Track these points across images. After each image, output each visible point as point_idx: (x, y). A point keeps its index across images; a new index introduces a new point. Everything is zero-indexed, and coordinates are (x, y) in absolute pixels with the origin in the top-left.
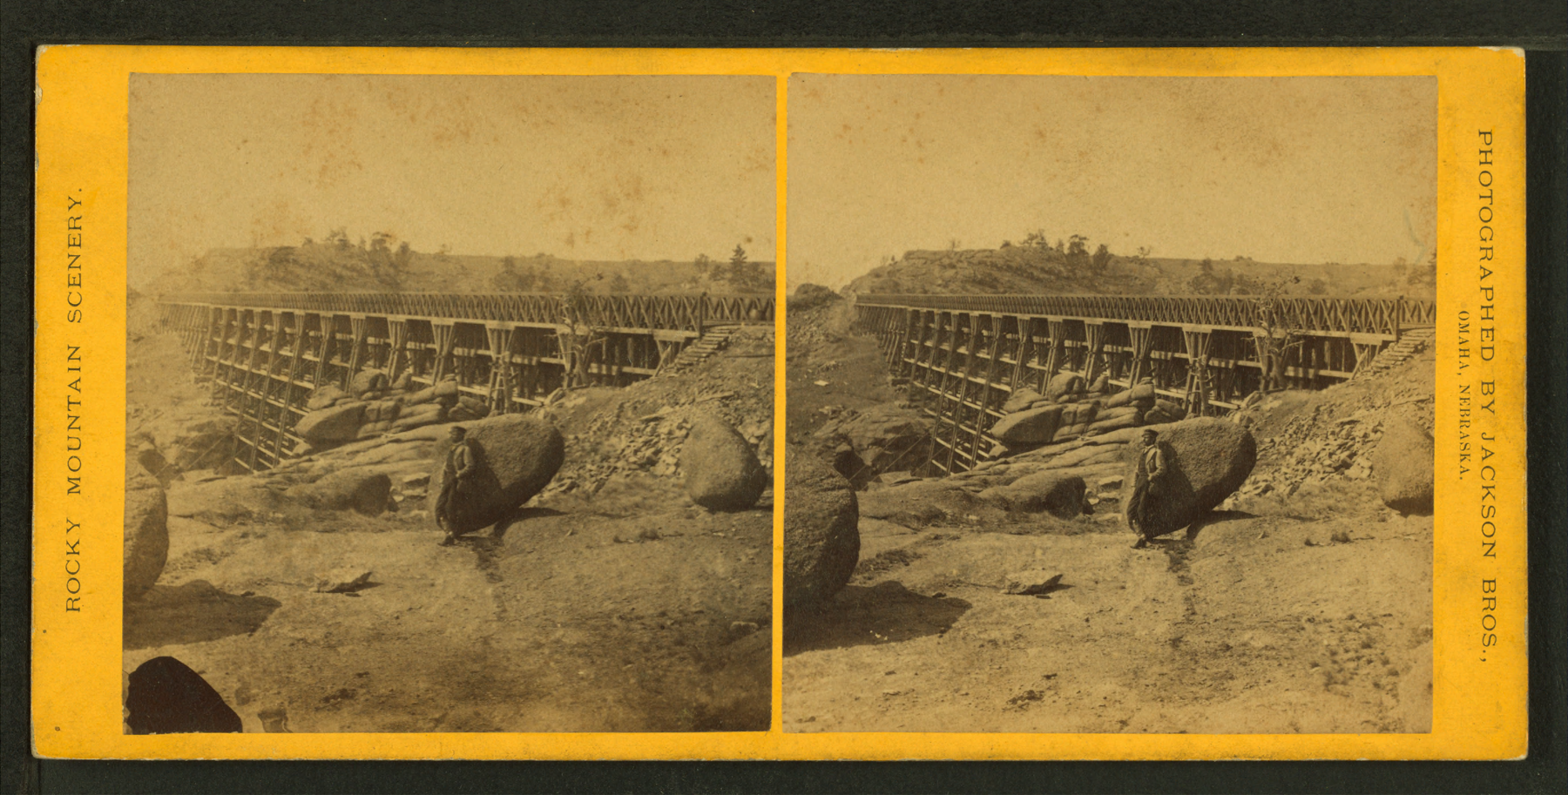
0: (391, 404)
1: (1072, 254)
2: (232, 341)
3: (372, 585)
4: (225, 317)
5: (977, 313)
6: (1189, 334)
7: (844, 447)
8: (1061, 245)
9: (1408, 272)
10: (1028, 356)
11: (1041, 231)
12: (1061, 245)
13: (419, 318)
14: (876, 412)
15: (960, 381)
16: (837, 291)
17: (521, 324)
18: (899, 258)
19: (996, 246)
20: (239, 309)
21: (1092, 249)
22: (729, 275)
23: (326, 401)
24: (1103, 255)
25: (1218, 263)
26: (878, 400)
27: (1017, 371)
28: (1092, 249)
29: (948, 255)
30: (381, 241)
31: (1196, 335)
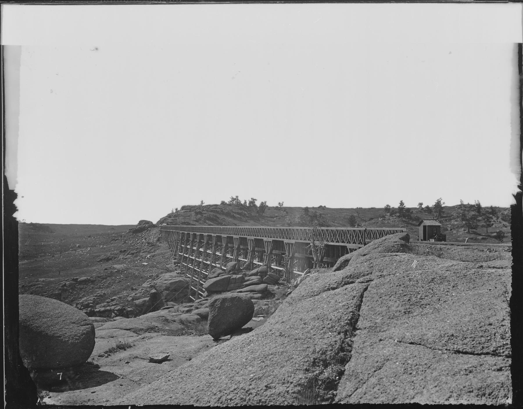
0: (241, 276)
1: (250, 206)
2: (195, 248)
3: (169, 360)
4: (198, 237)
5: (206, 234)
6: (266, 242)
7: (154, 291)
8: (245, 202)
9: (391, 211)
10: (226, 252)
11: (237, 197)
12: (245, 202)
13: (259, 238)
14: (167, 275)
15: (208, 265)
16: (155, 222)
17: (297, 241)
18: (179, 209)
19: (219, 203)
20: (198, 233)
21: (258, 204)
22: (398, 214)
23: (215, 275)
24: (263, 206)
25: (311, 208)
26: (168, 271)
27: (222, 258)
28: (258, 204)
29: (199, 207)
30: (253, 202)
31: (289, 244)
